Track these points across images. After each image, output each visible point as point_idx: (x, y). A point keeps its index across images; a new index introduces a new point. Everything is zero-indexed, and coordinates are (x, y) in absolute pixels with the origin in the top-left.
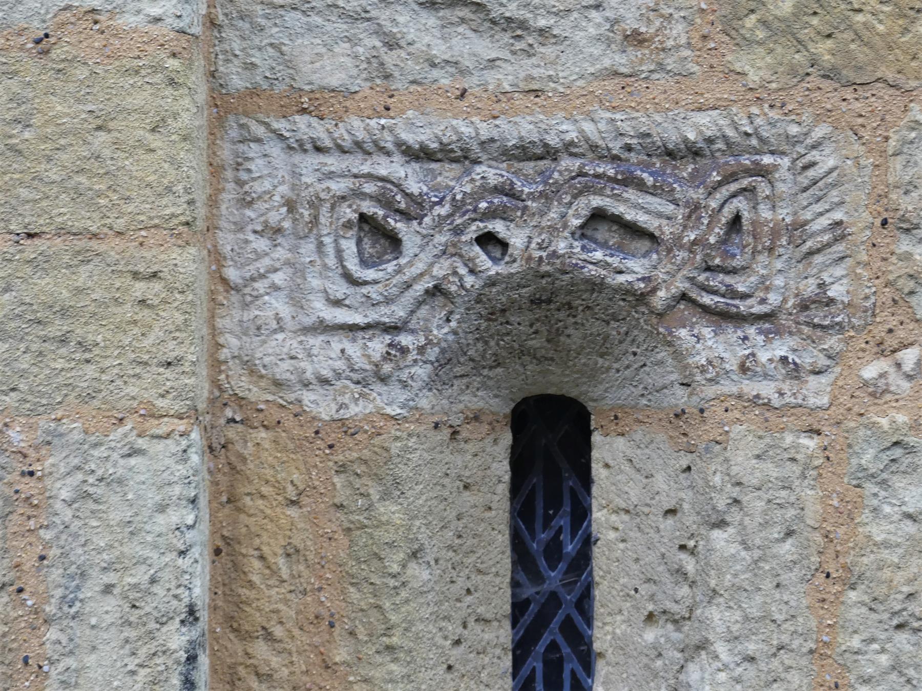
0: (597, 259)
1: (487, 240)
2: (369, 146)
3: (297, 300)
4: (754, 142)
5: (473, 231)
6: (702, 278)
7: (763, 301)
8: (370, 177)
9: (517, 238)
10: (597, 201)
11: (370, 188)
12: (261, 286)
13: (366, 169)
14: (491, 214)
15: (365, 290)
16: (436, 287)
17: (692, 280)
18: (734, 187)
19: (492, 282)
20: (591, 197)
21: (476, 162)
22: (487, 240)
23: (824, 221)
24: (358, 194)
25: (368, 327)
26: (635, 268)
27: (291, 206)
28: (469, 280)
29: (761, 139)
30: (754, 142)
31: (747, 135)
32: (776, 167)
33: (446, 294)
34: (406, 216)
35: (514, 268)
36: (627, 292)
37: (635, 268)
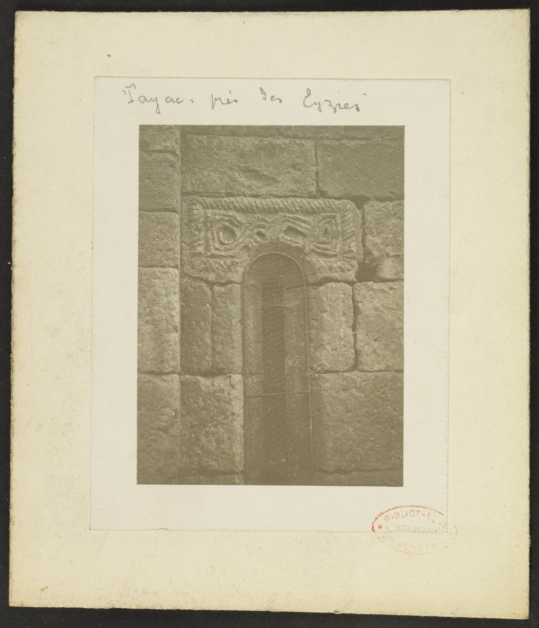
0: (288, 239)
1: (260, 234)
2: (226, 208)
3: (207, 248)
4: (330, 209)
5: (256, 231)
6: (317, 245)
7: (335, 251)
8: (226, 215)
9: (268, 234)
10: (290, 224)
11: (226, 218)
12: (196, 244)
13: (225, 213)
14: (260, 226)
15: (226, 246)
16: (245, 246)
17: (315, 246)
18: (325, 221)
19: (261, 245)
20: (325, 357)
21: (255, 213)
22: (260, 234)
23: (349, 231)
24: (223, 220)
25: (339, 281)
26: (300, 241)
27: (205, 223)
28: (254, 244)
29: (332, 208)
30: (330, 209)
31: (329, 207)
32: (336, 216)
33: (248, 248)
34: (237, 226)
35: (266, 242)
36: (298, 248)
37: (300, 241)
